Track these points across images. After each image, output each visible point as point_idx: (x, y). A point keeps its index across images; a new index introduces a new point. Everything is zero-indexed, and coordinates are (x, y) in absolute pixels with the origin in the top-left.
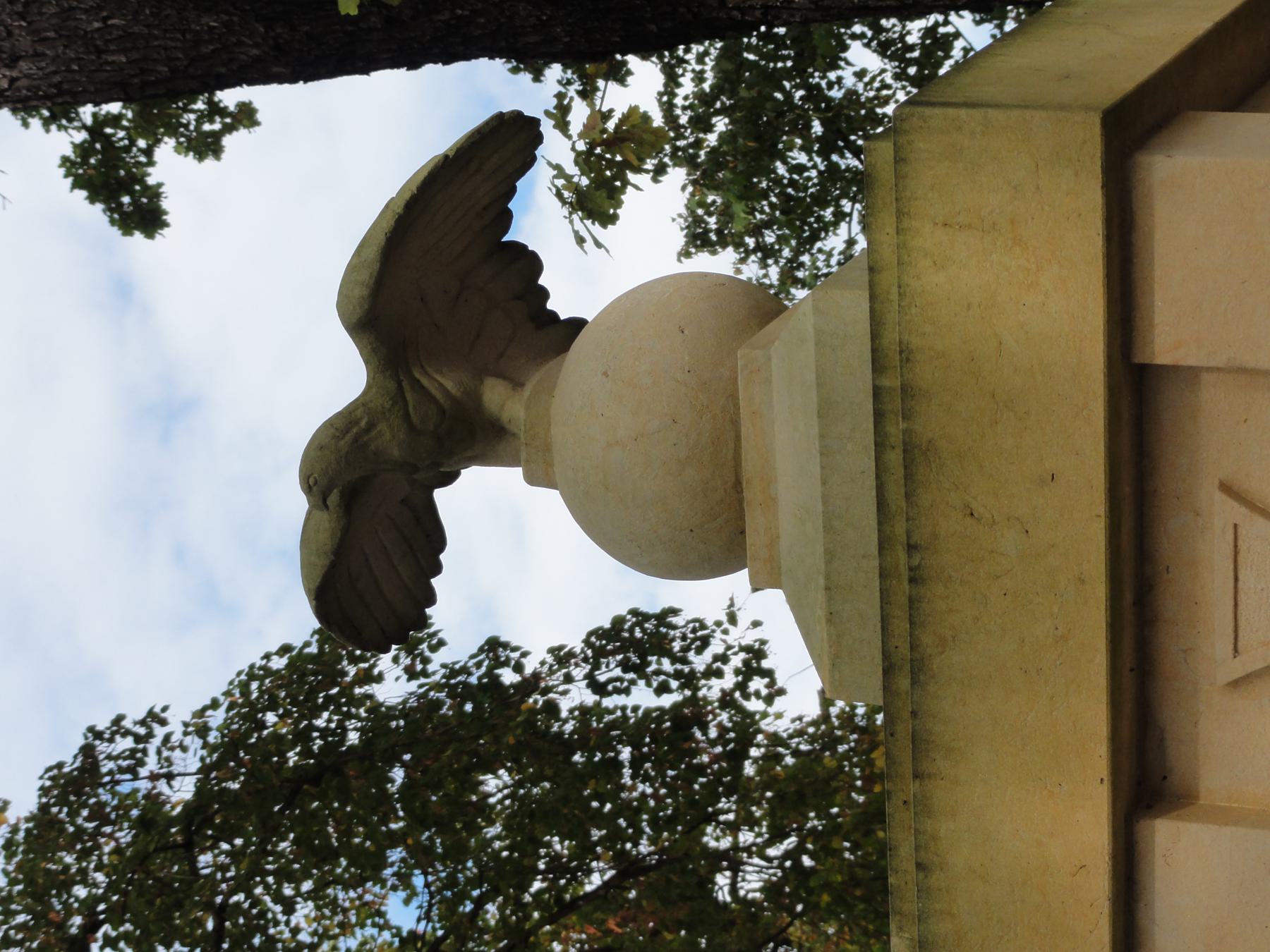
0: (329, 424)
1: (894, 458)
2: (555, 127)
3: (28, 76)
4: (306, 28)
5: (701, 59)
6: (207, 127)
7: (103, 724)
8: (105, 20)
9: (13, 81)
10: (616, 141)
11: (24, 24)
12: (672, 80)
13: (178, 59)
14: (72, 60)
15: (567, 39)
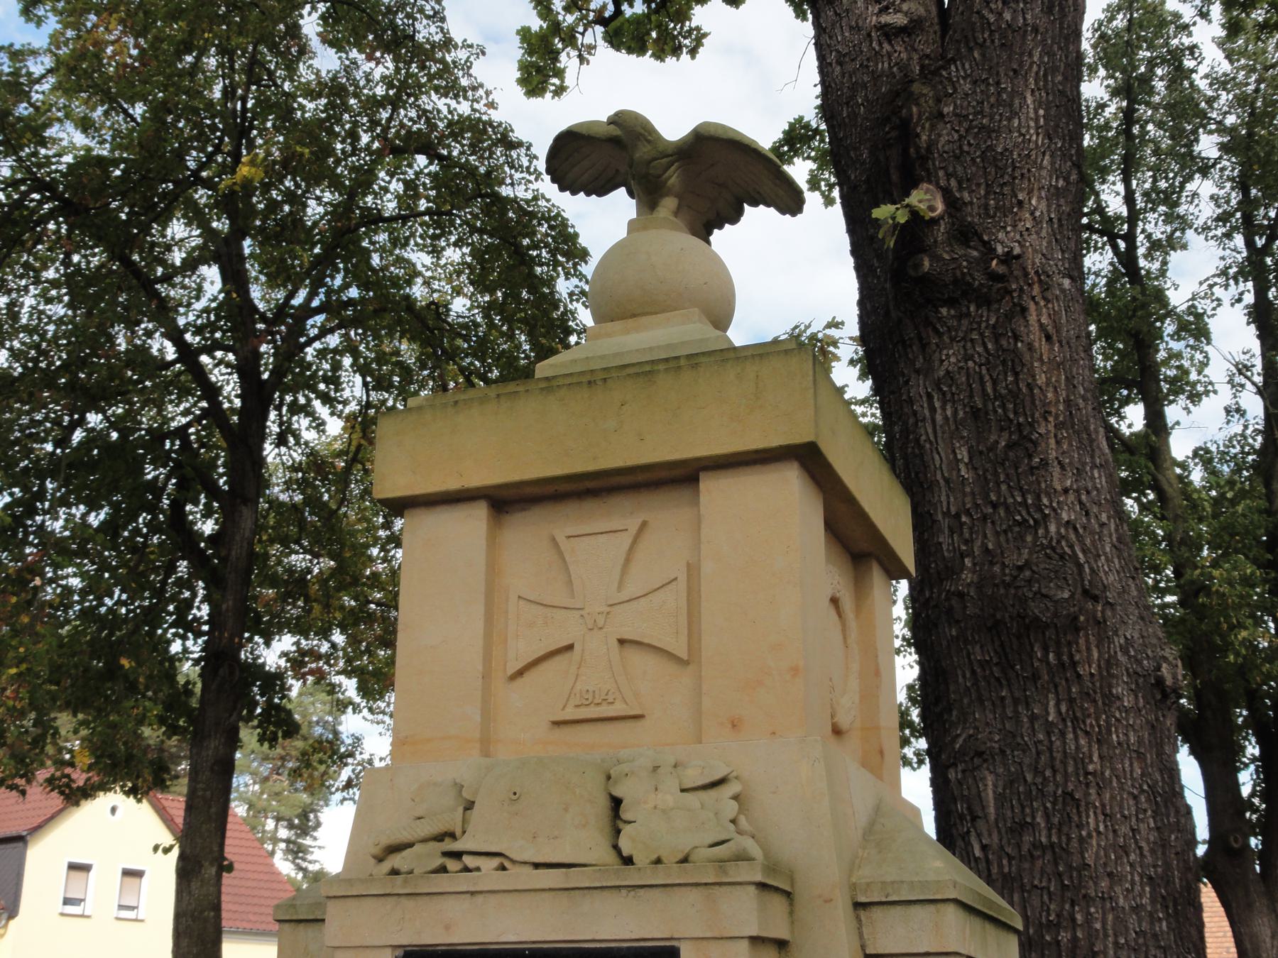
0: (648, 122)
1: (648, 368)
5: (873, 415)
6: (823, 183)
7: (534, 150)
9: (830, 64)
10: (824, 352)
12: (863, 402)
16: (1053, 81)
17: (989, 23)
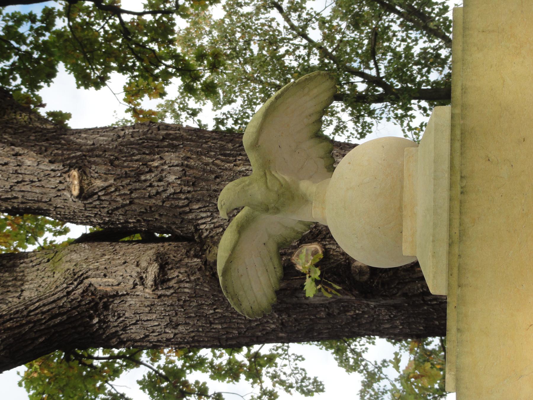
2: (393, 367)
3: (181, 333)
4: (294, 316)
8: (215, 309)
9: (175, 334)
11: (183, 310)
13: (242, 328)
14: (200, 326)
15: (401, 327)
16: (231, 150)
17: (174, 193)
